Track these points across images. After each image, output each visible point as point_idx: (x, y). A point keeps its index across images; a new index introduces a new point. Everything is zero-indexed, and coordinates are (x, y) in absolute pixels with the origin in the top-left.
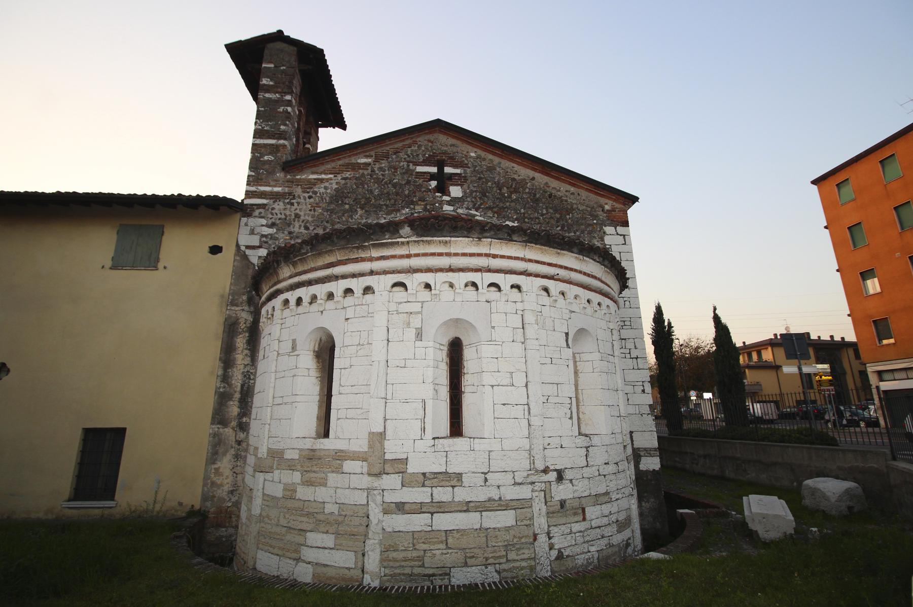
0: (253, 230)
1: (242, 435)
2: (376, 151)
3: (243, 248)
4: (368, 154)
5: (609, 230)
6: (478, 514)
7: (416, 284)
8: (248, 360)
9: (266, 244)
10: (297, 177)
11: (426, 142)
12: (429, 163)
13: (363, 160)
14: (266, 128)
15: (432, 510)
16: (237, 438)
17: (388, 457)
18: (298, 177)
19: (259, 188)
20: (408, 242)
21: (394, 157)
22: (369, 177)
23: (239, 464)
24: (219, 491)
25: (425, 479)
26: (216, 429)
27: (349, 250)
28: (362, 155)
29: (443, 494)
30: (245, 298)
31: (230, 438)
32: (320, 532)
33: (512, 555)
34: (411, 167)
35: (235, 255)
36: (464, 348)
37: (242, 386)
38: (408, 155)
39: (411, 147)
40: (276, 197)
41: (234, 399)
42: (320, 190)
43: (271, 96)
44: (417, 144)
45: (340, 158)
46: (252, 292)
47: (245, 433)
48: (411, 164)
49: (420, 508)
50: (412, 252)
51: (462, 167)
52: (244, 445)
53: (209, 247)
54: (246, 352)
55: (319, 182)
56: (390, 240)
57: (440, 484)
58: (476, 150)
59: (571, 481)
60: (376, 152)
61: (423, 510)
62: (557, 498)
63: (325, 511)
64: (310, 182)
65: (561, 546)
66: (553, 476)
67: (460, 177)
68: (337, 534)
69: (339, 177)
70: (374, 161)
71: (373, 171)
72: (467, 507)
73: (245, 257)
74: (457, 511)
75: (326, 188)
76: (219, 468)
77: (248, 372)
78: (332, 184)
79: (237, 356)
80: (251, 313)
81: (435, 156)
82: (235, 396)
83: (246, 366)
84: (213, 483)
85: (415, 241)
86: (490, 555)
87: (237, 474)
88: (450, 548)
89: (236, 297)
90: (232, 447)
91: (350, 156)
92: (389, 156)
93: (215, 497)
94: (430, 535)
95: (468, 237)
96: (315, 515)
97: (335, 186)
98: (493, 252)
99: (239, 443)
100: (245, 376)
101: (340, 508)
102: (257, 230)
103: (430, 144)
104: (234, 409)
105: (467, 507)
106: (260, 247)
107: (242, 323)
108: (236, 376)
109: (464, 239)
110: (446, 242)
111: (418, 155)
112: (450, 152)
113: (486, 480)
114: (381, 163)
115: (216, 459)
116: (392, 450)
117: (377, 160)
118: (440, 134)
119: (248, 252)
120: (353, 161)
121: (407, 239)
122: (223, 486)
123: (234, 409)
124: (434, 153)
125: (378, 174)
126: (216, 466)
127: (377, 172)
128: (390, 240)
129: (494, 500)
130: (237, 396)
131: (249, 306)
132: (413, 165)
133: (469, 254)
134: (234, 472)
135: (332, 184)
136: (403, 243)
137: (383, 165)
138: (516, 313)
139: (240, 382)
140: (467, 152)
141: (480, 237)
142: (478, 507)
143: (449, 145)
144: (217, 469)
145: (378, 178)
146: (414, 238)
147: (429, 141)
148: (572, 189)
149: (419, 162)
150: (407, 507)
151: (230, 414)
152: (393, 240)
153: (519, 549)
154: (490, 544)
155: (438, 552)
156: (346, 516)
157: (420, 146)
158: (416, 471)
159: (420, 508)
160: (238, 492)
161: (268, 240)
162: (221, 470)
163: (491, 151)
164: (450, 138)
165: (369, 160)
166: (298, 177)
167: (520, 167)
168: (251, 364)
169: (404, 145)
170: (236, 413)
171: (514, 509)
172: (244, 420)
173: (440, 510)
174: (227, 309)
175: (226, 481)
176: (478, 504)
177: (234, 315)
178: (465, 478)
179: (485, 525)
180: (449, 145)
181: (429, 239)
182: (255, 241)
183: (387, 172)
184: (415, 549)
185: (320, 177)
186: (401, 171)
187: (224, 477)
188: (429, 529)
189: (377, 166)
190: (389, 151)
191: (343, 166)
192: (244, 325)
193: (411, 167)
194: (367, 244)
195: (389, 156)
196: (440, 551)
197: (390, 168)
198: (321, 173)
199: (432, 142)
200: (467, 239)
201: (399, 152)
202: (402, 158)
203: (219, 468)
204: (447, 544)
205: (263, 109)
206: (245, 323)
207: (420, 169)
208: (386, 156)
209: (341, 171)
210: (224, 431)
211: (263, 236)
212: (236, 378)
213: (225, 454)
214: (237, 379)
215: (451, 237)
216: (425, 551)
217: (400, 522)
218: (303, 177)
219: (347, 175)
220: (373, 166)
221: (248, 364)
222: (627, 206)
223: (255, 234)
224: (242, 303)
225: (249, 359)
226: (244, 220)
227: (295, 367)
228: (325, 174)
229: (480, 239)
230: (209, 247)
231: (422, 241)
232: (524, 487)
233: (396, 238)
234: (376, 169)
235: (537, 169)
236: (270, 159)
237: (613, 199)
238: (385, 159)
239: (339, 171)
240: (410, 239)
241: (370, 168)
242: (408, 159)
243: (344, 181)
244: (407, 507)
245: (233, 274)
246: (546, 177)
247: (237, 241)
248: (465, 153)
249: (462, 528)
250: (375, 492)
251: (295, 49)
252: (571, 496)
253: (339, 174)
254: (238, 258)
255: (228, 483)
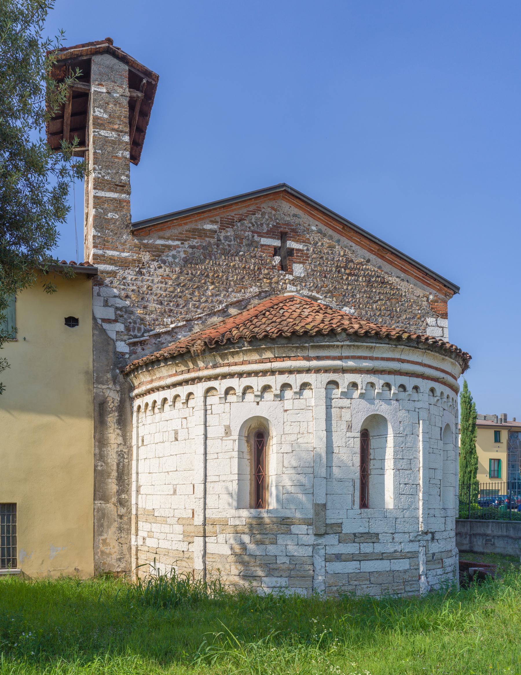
0: (107, 301)
1: (122, 510)
2: (222, 216)
3: (99, 321)
4: (213, 219)
5: (430, 320)
6: (388, 561)
7: (346, 384)
8: (120, 440)
9: (121, 318)
10: (144, 241)
11: (269, 210)
12: (273, 235)
13: (209, 227)
14: (106, 178)
15: (360, 558)
16: (119, 513)
17: (328, 521)
18: (145, 241)
19: (107, 252)
20: (342, 346)
21: (239, 224)
22: (215, 246)
23: (123, 535)
24: (109, 559)
25: (356, 537)
26: (99, 505)
27: (288, 349)
28: (208, 221)
29: (367, 548)
30: (109, 376)
31: (112, 513)
32: (275, 577)
33: (408, 588)
34: (256, 238)
35: (93, 329)
36: (371, 438)
37: (118, 465)
38: (252, 223)
39: (255, 214)
40: (124, 264)
41: (112, 477)
42: (169, 258)
43: (107, 135)
44: (261, 211)
45: (187, 223)
46: (115, 370)
47: (125, 508)
48: (256, 235)
49: (352, 558)
50: (343, 355)
51: (304, 242)
52: (125, 519)
53: (65, 318)
54: (118, 431)
55: (167, 250)
56: (328, 343)
57: (365, 541)
58: (317, 223)
59: (437, 540)
60: (221, 218)
61: (354, 559)
62: (431, 552)
63: (278, 562)
64: (158, 249)
65: (432, 583)
66: (429, 536)
67: (302, 254)
68: (290, 577)
69: (186, 244)
70: (220, 229)
71: (219, 240)
72: (382, 556)
73: (103, 331)
74: (376, 559)
75: (174, 257)
76: (106, 539)
77: (121, 451)
78: (179, 252)
79: (110, 435)
80: (118, 392)
81: (278, 227)
82: (112, 474)
83: (119, 445)
84: (102, 552)
85: (348, 346)
86: (396, 588)
87: (122, 544)
88: (372, 584)
89: (101, 375)
90: (115, 521)
91: (196, 221)
92: (235, 224)
93: (106, 564)
94: (359, 576)
95: (388, 344)
96: (268, 565)
97: (183, 255)
98: (403, 357)
99: (121, 517)
100: (119, 455)
101: (290, 559)
102: (111, 301)
103: (273, 212)
104: (113, 486)
105: (382, 556)
106: (116, 321)
107: (110, 402)
108: (111, 455)
109: (385, 345)
110: (372, 348)
111: (262, 224)
112: (292, 224)
113: (393, 539)
114: (227, 232)
115: (102, 531)
116: (332, 517)
117: (223, 228)
118: (283, 201)
119: (106, 326)
120: (199, 227)
121: (342, 343)
122: (111, 555)
123: (113, 486)
124: (277, 223)
125: (224, 243)
126: (103, 538)
127: (223, 241)
128: (328, 343)
129: (398, 552)
130: (114, 474)
131: (115, 383)
132: (258, 236)
133: (387, 358)
134: (120, 543)
135: (179, 252)
136: (338, 346)
137: (229, 234)
138: (415, 411)
139: (116, 460)
140: (309, 225)
141: (397, 344)
142: (389, 556)
143: (291, 214)
144: (104, 541)
145: (224, 249)
146: (348, 343)
147: (273, 208)
148: (402, 275)
149: (264, 233)
150: (343, 557)
151: (110, 490)
152: (331, 343)
153: (411, 584)
154: (395, 580)
155: (365, 586)
156: (296, 564)
157: (263, 214)
158: (348, 532)
159: (352, 558)
160: (125, 559)
161: (123, 313)
162: (108, 541)
163: (332, 226)
164: (292, 207)
165: (215, 227)
166: (145, 241)
167: (358, 247)
168: (123, 443)
169: (248, 211)
170: (115, 490)
171: (409, 558)
172: (123, 496)
173: (366, 559)
174: (94, 387)
175: (113, 551)
176: (389, 554)
177: (101, 394)
178: (380, 536)
179: (393, 568)
180: (291, 214)
181: (359, 344)
182: (110, 314)
183: (232, 243)
184: (350, 585)
185: (167, 243)
186: (247, 243)
187: (112, 547)
188: (358, 571)
189: (222, 235)
190: (234, 217)
191: (190, 231)
192: (112, 404)
193: (256, 238)
194: (307, 345)
195: (235, 224)
196: (366, 586)
197: (236, 237)
198: (168, 239)
199: (275, 210)
200: (387, 346)
201: (244, 220)
202: (246, 227)
203: (106, 539)
204: (370, 581)
205: (100, 151)
206: (113, 402)
207: (264, 241)
208: (232, 224)
209: (189, 237)
210: (107, 506)
211: (117, 309)
212: (112, 457)
213: (109, 527)
214: (112, 459)
215: (376, 343)
216: (356, 585)
217: (338, 567)
218: (150, 242)
219: (194, 243)
220: (219, 234)
221: (121, 444)
222: (448, 297)
223: (110, 306)
224: (107, 381)
225: (121, 438)
226: (96, 288)
227: (232, 450)
228: (173, 240)
229: (396, 345)
230: (65, 318)
231: (354, 345)
232: (415, 543)
233: (333, 342)
234: (222, 238)
235: (373, 251)
236: (114, 217)
237: (437, 288)
238: (231, 226)
239: (186, 237)
240: (345, 343)
241: (216, 236)
242: (252, 228)
243: (191, 249)
244: (343, 557)
245: (94, 349)
246: (380, 260)
247: (93, 313)
248: (306, 225)
249: (379, 570)
250: (319, 547)
251: (127, 68)
252: (437, 551)
253: (186, 240)
254: (96, 332)
255: (115, 552)
